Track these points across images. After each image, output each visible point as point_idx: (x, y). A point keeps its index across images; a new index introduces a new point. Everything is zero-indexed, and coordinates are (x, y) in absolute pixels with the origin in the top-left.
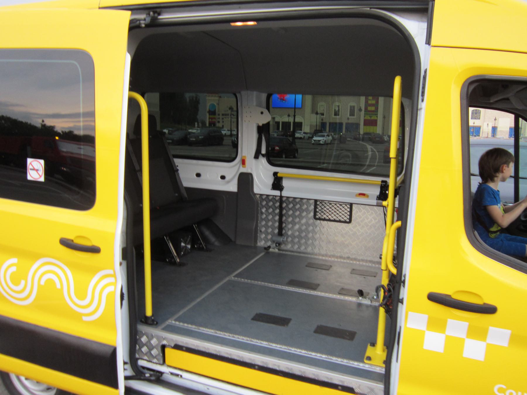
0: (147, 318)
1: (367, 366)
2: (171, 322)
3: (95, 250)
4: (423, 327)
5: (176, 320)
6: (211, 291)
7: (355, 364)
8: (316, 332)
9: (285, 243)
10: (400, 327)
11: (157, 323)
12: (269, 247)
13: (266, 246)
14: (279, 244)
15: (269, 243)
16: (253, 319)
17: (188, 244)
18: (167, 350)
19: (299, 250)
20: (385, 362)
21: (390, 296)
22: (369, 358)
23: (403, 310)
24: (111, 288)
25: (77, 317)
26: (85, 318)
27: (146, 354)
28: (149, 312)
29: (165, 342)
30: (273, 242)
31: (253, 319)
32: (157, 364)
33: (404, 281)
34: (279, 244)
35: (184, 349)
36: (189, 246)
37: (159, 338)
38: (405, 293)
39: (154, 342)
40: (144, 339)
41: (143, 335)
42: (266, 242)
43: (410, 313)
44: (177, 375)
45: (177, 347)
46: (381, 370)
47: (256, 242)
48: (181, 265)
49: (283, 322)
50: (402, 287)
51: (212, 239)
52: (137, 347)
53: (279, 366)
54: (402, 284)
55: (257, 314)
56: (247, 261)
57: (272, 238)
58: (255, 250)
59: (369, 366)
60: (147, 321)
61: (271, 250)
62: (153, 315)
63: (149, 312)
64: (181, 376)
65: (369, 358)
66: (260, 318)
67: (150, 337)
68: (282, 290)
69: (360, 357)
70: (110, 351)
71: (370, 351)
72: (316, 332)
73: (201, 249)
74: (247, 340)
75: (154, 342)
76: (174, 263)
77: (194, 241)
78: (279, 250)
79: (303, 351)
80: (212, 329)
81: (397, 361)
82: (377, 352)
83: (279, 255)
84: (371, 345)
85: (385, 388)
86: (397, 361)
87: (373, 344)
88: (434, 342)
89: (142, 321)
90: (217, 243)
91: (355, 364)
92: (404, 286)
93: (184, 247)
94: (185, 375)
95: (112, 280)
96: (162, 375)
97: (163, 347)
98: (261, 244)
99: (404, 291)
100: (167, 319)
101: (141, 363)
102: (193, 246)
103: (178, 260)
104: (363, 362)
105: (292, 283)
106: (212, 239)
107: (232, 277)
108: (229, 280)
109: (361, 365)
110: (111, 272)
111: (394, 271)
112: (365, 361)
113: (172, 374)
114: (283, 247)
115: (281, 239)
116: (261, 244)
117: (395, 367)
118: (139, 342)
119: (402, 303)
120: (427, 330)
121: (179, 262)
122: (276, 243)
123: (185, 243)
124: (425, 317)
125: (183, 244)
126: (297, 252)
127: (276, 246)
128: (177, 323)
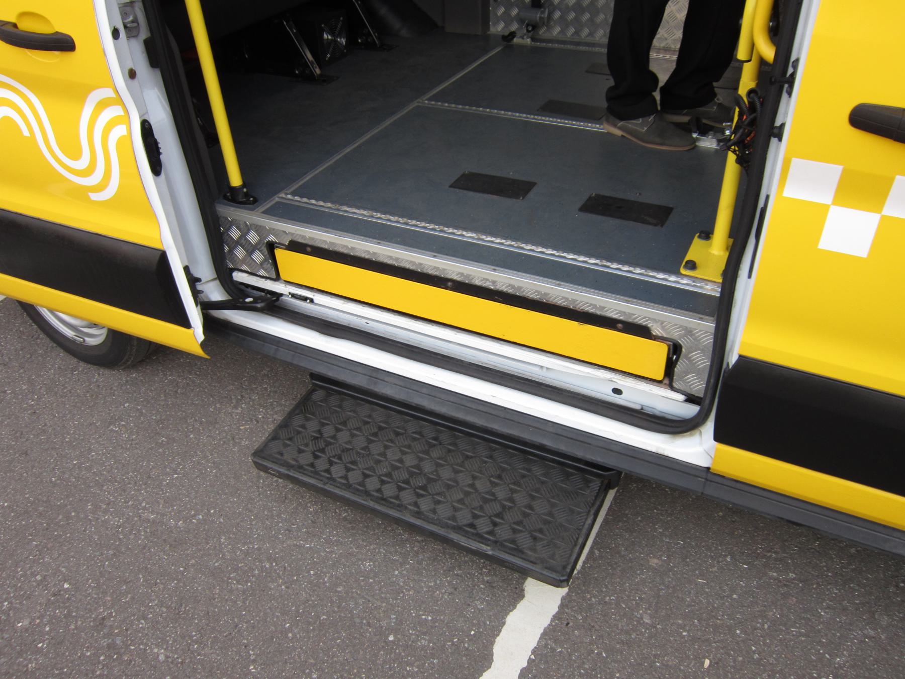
0: (233, 190)
1: (685, 281)
2: (286, 196)
3: (62, 44)
4: (825, 197)
5: (294, 194)
6: (375, 131)
7: (659, 277)
8: (585, 208)
9: (547, 22)
10: (768, 197)
11: (256, 201)
12: (512, 35)
13: (506, 34)
14: (533, 27)
15: (514, 27)
16: (451, 186)
17: (340, 35)
18: (280, 253)
19: (576, 39)
20: (725, 274)
21: (753, 123)
22: (692, 265)
23: (779, 154)
24: (120, 131)
25: (81, 194)
26: (94, 197)
27: (243, 261)
28: (235, 179)
29: (272, 238)
30: (521, 21)
31: (451, 186)
32: (266, 278)
33: (793, 76)
34: (533, 27)
35: (309, 249)
36: (343, 41)
37: (259, 229)
38: (794, 112)
39: (253, 237)
40: (235, 234)
41: (232, 224)
42: (507, 25)
43: (795, 161)
44: (305, 299)
45: (296, 247)
46: (713, 290)
47: (486, 22)
48: (324, 80)
49: (516, 189)
50: (785, 95)
51: (395, 23)
52: (226, 248)
53: (494, 282)
54: (786, 86)
55: (463, 175)
56: (463, 67)
57: (518, 14)
58: (485, 41)
59: (690, 282)
60: (245, 198)
61: (516, 40)
62: (245, 185)
63: (235, 179)
64: (312, 301)
65: (692, 265)
66: (471, 182)
67: (245, 230)
68: (527, 123)
69: (674, 260)
70: (158, 255)
71: (696, 250)
72: (585, 208)
73: (370, 46)
74: (434, 230)
75: (253, 237)
76: (310, 78)
77: (353, 29)
78: (533, 39)
79: (550, 252)
80: (365, 209)
81: (750, 277)
82: (711, 253)
83: (534, 50)
84: (699, 237)
85: (717, 328)
86: (750, 277)
87: (707, 235)
88: (849, 232)
89: (225, 198)
90: (404, 33)
91: (659, 277)
92: (790, 94)
93: (329, 42)
94: (318, 298)
95: (115, 111)
96: (278, 299)
97: (271, 247)
98: (498, 28)
99: (788, 103)
100: (276, 192)
101: (238, 277)
102: (351, 42)
103: (318, 71)
104: (677, 273)
105: (553, 108)
106: (395, 23)
107: (424, 101)
108: (418, 107)
109: (671, 280)
110: (109, 93)
111: (768, 52)
112: (683, 271)
113: (294, 296)
114: (542, 32)
115: (537, 15)
116: (498, 28)
117: (744, 288)
118: (225, 237)
119: (780, 137)
120: (835, 202)
121: (321, 75)
122: (527, 25)
123: (332, 33)
124: (834, 171)
125: (326, 36)
126: (572, 43)
127: (528, 31)
128: (297, 198)
